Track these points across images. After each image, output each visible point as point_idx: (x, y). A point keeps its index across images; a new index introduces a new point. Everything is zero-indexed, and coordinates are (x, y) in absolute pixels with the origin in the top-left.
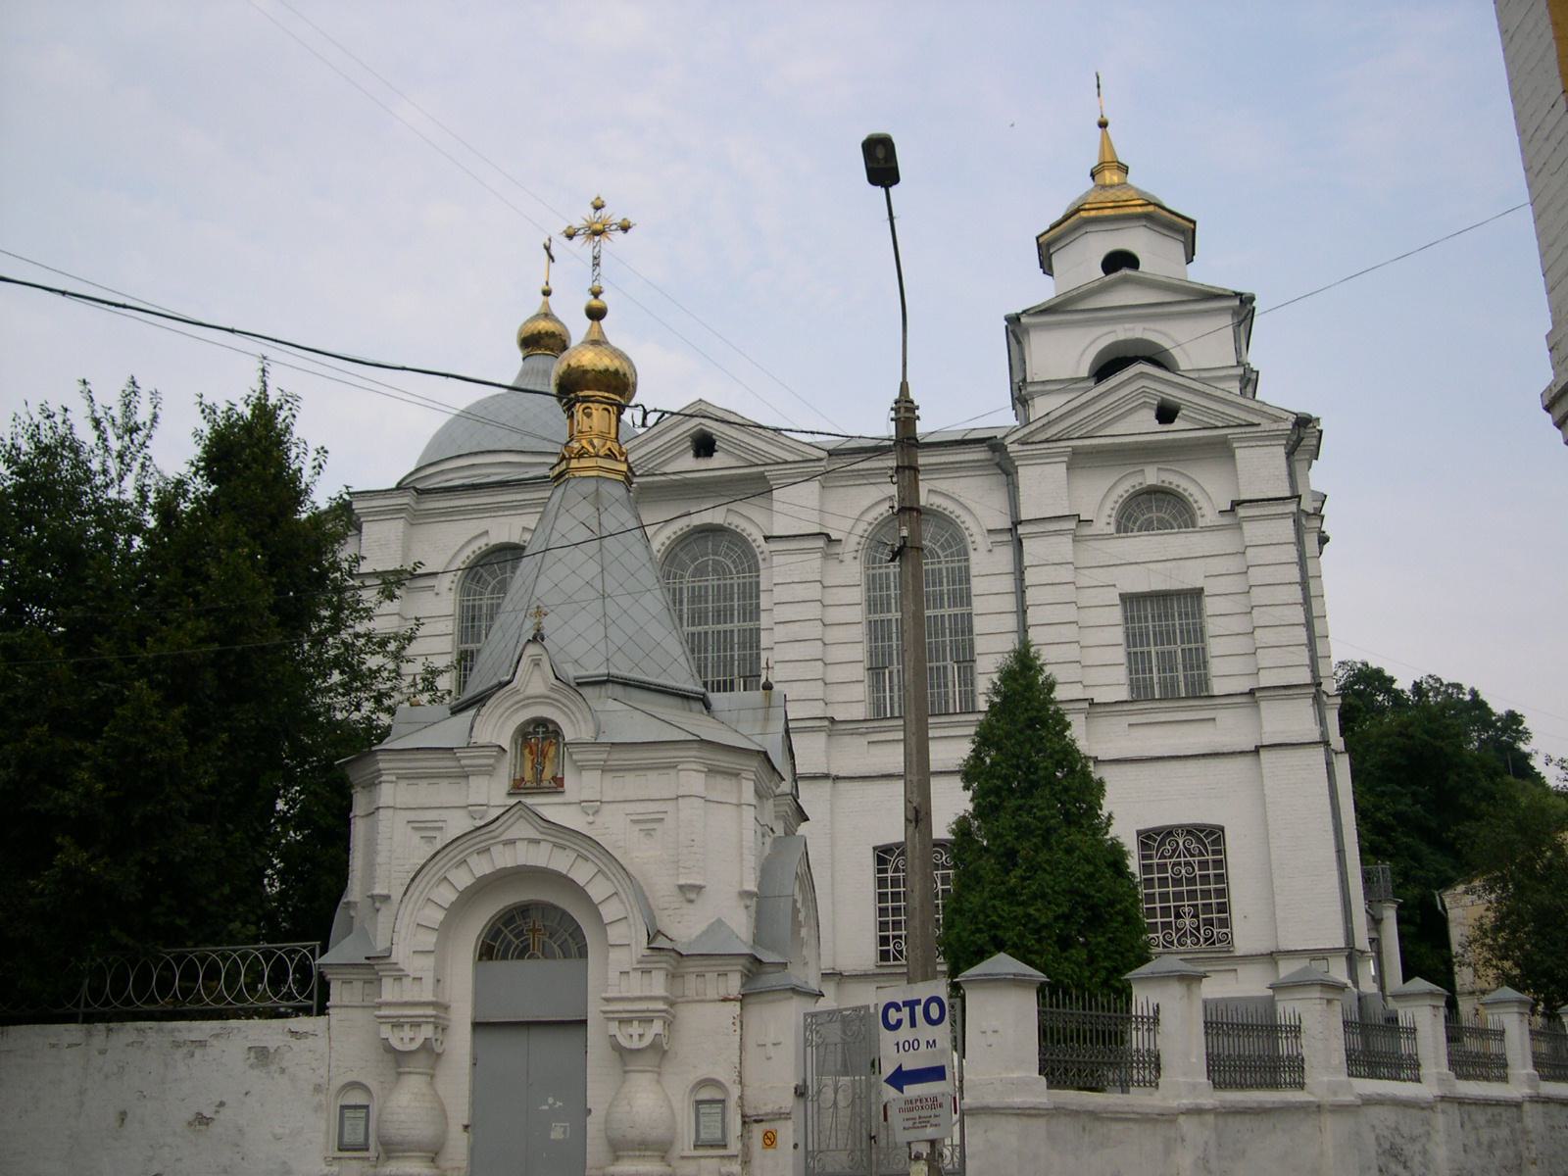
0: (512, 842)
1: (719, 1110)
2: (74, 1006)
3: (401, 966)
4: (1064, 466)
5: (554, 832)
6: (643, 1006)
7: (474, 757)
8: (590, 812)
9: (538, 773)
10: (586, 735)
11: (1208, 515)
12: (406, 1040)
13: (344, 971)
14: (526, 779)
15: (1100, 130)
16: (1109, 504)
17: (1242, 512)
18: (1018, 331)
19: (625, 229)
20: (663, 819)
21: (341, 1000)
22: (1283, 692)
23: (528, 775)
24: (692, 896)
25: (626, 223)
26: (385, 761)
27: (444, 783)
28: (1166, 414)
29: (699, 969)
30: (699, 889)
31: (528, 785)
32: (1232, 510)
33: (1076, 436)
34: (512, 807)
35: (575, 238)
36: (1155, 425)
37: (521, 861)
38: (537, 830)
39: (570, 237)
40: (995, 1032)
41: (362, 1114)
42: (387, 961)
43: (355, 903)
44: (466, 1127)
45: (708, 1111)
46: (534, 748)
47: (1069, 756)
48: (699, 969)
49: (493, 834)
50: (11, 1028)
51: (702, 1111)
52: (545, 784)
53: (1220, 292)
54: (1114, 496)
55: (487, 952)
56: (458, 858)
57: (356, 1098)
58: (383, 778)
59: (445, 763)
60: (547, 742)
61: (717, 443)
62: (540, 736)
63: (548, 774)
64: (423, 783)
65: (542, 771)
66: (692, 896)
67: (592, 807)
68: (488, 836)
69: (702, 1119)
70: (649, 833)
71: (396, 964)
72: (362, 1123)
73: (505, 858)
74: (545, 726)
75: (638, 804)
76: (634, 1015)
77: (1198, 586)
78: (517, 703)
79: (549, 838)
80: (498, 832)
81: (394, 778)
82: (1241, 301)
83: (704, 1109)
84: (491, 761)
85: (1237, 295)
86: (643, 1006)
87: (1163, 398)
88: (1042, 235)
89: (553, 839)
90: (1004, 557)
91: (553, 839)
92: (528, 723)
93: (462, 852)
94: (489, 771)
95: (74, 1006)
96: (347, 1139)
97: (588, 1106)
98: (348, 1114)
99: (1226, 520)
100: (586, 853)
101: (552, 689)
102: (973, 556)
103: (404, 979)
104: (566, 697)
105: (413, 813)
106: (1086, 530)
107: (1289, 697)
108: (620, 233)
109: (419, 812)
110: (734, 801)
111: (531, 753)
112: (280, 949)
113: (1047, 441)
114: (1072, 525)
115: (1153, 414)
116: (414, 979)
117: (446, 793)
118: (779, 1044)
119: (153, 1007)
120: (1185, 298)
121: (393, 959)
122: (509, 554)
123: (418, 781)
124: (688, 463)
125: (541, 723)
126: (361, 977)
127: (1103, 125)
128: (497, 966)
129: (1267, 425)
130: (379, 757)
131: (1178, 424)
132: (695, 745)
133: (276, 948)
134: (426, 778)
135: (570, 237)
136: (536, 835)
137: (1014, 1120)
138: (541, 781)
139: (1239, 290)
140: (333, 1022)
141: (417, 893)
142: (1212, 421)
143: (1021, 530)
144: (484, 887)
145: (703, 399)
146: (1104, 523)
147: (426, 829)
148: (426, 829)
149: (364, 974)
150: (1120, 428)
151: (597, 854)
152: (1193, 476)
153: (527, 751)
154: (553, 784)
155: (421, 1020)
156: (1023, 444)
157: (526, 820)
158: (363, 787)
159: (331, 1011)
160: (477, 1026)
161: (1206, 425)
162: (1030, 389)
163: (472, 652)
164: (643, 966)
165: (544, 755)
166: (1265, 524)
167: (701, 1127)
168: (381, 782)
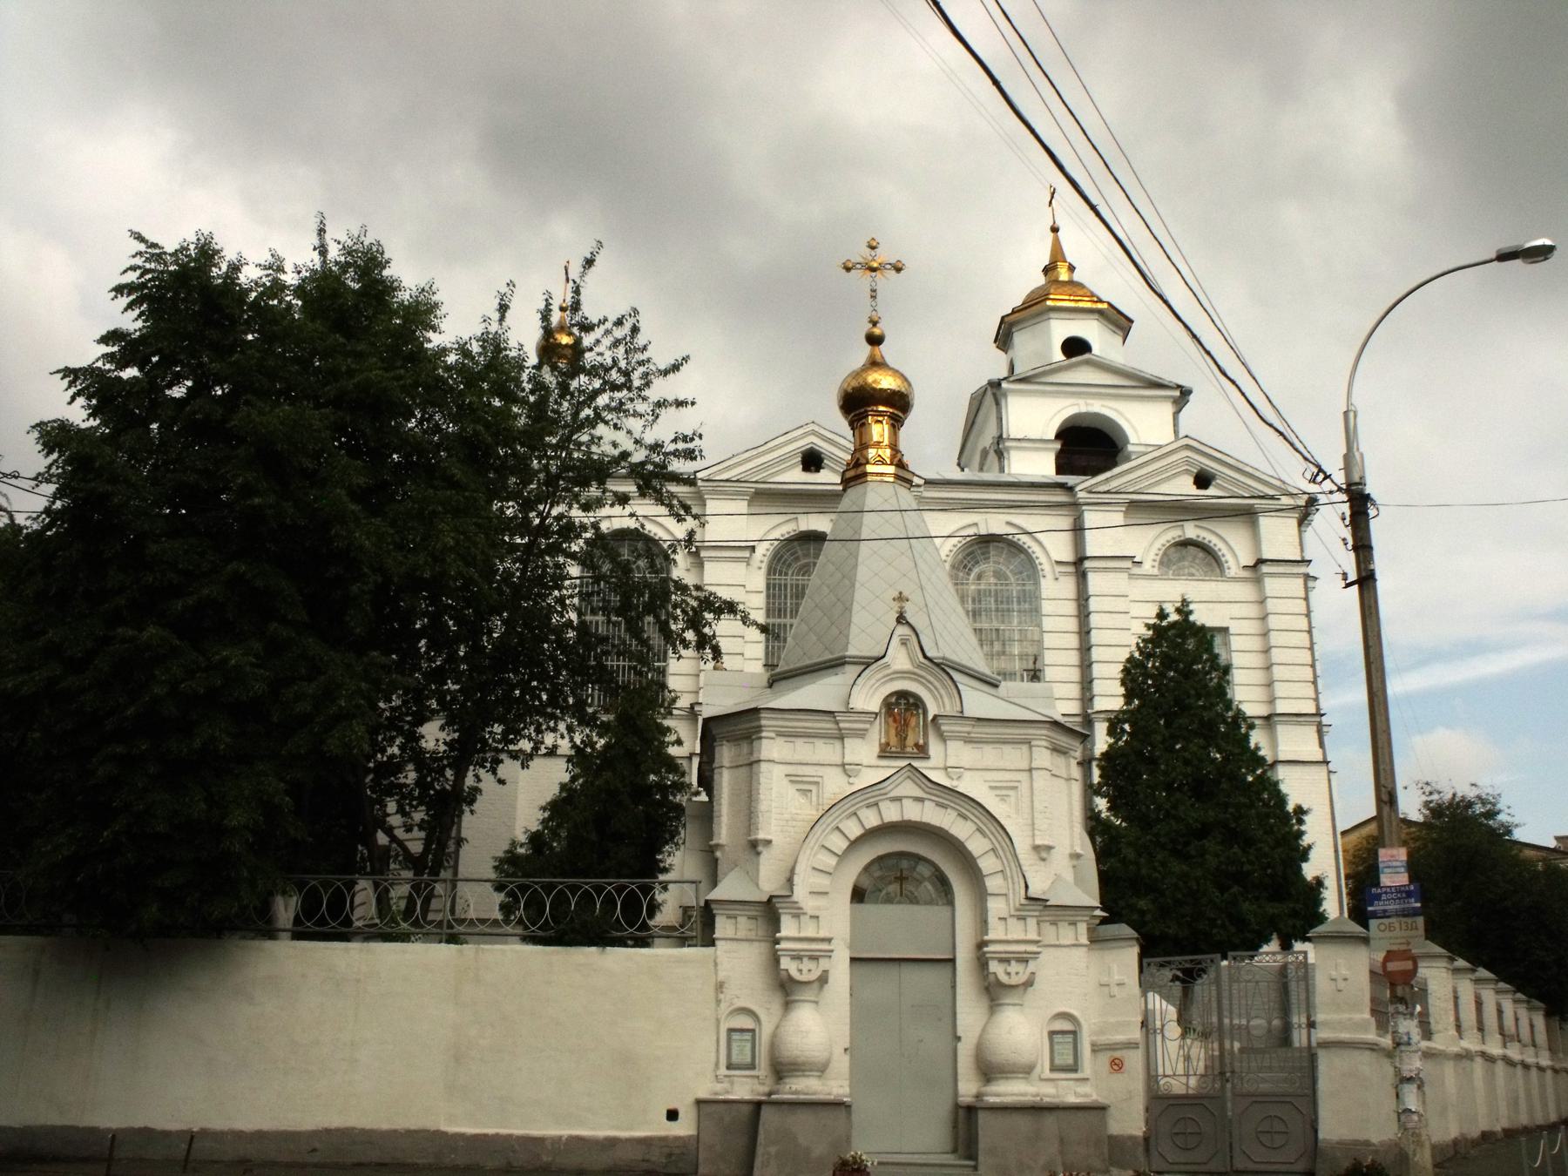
0: (898, 799)
1: (1071, 1040)
2: (340, 924)
3: (801, 905)
4: (746, 502)
5: (938, 793)
6: (1022, 948)
7: (856, 721)
8: (955, 777)
9: (903, 740)
10: (950, 708)
11: (1233, 569)
12: (805, 971)
13: (726, 907)
14: (891, 744)
15: (1052, 234)
16: (1154, 550)
17: (1265, 569)
18: (998, 393)
19: (898, 270)
20: (1017, 787)
21: (1006, 934)
22: (1295, 719)
23: (894, 740)
24: (1044, 855)
25: (900, 265)
26: (769, 719)
27: (819, 743)
28: (1203, 480)
29: (1071, 918)
30: (1049, 848)
31: (893, 749)
32: (1255, 566)
33: (1131, 490)
34: (902, 768)
35: (853, 271)
36: (1194, 490)
37: (926, 819)
38: (923, 790)
39: (848, 269)
40: (1345, 979)
41: (748, 1036)
42: (788, 900)
43: (722, 846)
44: (846, 1050)
45: (1061, 1040)
46: (898, 718)
47: (1256, 760)
48: (1071, 918)
49: (882, 791)
50: (608, 948)
51: (1056, 1040)
52: (909, 749)
53: (1166, 383)
54: (1158, 545)
55: (858, 895)
56: (850, 810)
57: (745, 1022)
58: (764, 734)
59: (826, 725)
60: (908, 714)
61: (825, 461)
62: (902, 707)
63: (910, 741)
64: (800, 741)
65: (905, 739)
66: (1044, 855)
67: (957, 773)
68: (878, 792)
69: (1056, 1047)
70: (805, 792)
71: (797, 903)
72: (749, 1045)
73: (891, 814)
74: (906, 699)
75: (995, 772)
76: (1012, 955)
77: (1224, 625)
78: (888, 675)
79: (933, 798)
80: (889, 788)
81: (773, 735)
82: (1181, 392)
83: (1058, 1038)
84: (867, 726)
85: (1179, 387)
86: (1022, 948)
87: (801, 452)
88: (1008, 315)
89: (937, 799)
90: (1068, 587)
91: (937, 799)
92: (891, 695)
93: (853, 805)
94: (861, 734)
95: (340, 924)
96: (1058, 1062)
97: (959, 1034)
98: (736, 1036)
99: (1246, 574)
100: (967, 813)
101: (919, 667)
102: (1043, 582)
103: (802, 917)
104: (932, 674)
105: (794, 767)
106: (1136, 570)
107: (1299, 723)
108: (894, 272)
109: (799, 767)
110: (1065, 776)
111: (895, 721)
112: (587, 884)
113: (1108, 492)
114: (1128, 564)
115: (1191, 480)
116: (811, 917)
117: (825, 751)
118: (1123, 984)
119: (325, 929)
120: (1133, 384)
121: (795, 898)
122: (817, 538)
123: (815, 740)
124: (796, 476)
125: (902, 695)
126: (747, 913)
127: (1055, 230)
128: (869, 909)
129: (1285, 500)
130: (762, 715)
131: (1211, 491)
132: (1048, 726)
133: (533, 882)
134: (801, 736)
135: (848, 269)
136: (919, 793)
137: (1368, 1053)
138: (905, 747)
139: (1180, 383)
140: (719, 953)
141: (814, 840)
142: (1240, 492)
143: (1087, 564)
144: (871, 835)
145: (1189, 435)
146: (1148, 567)
147: (802, 782)
148: (802, 782)
149: (748, 910)
150: (1164, 488)
151: (978, 814)
152: (1223, 535)
153: (891, 720)
154: (915, 750)
155: (818, 953)
156: (1090, 492)
157: (913, 780)
158: (728, 741)
159: (717, 943)
160: (854, 960)
161: (1257, 493)
162: (1008, 444)
163: (785, 625)
164: (1018, 913)
165: (906, 724)
166: (1283, 580)
167: (1056, 1055)
168: (761, 738)
